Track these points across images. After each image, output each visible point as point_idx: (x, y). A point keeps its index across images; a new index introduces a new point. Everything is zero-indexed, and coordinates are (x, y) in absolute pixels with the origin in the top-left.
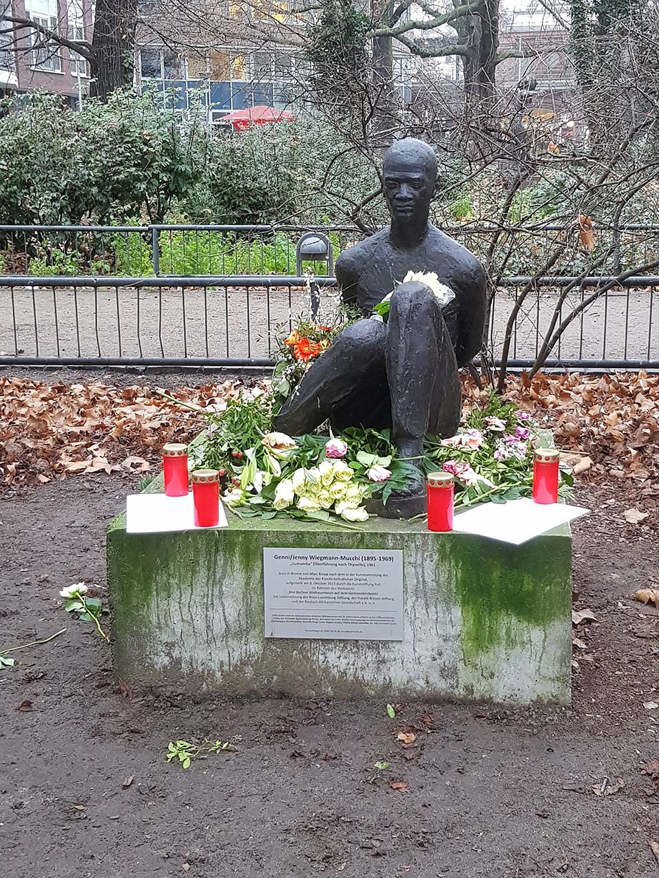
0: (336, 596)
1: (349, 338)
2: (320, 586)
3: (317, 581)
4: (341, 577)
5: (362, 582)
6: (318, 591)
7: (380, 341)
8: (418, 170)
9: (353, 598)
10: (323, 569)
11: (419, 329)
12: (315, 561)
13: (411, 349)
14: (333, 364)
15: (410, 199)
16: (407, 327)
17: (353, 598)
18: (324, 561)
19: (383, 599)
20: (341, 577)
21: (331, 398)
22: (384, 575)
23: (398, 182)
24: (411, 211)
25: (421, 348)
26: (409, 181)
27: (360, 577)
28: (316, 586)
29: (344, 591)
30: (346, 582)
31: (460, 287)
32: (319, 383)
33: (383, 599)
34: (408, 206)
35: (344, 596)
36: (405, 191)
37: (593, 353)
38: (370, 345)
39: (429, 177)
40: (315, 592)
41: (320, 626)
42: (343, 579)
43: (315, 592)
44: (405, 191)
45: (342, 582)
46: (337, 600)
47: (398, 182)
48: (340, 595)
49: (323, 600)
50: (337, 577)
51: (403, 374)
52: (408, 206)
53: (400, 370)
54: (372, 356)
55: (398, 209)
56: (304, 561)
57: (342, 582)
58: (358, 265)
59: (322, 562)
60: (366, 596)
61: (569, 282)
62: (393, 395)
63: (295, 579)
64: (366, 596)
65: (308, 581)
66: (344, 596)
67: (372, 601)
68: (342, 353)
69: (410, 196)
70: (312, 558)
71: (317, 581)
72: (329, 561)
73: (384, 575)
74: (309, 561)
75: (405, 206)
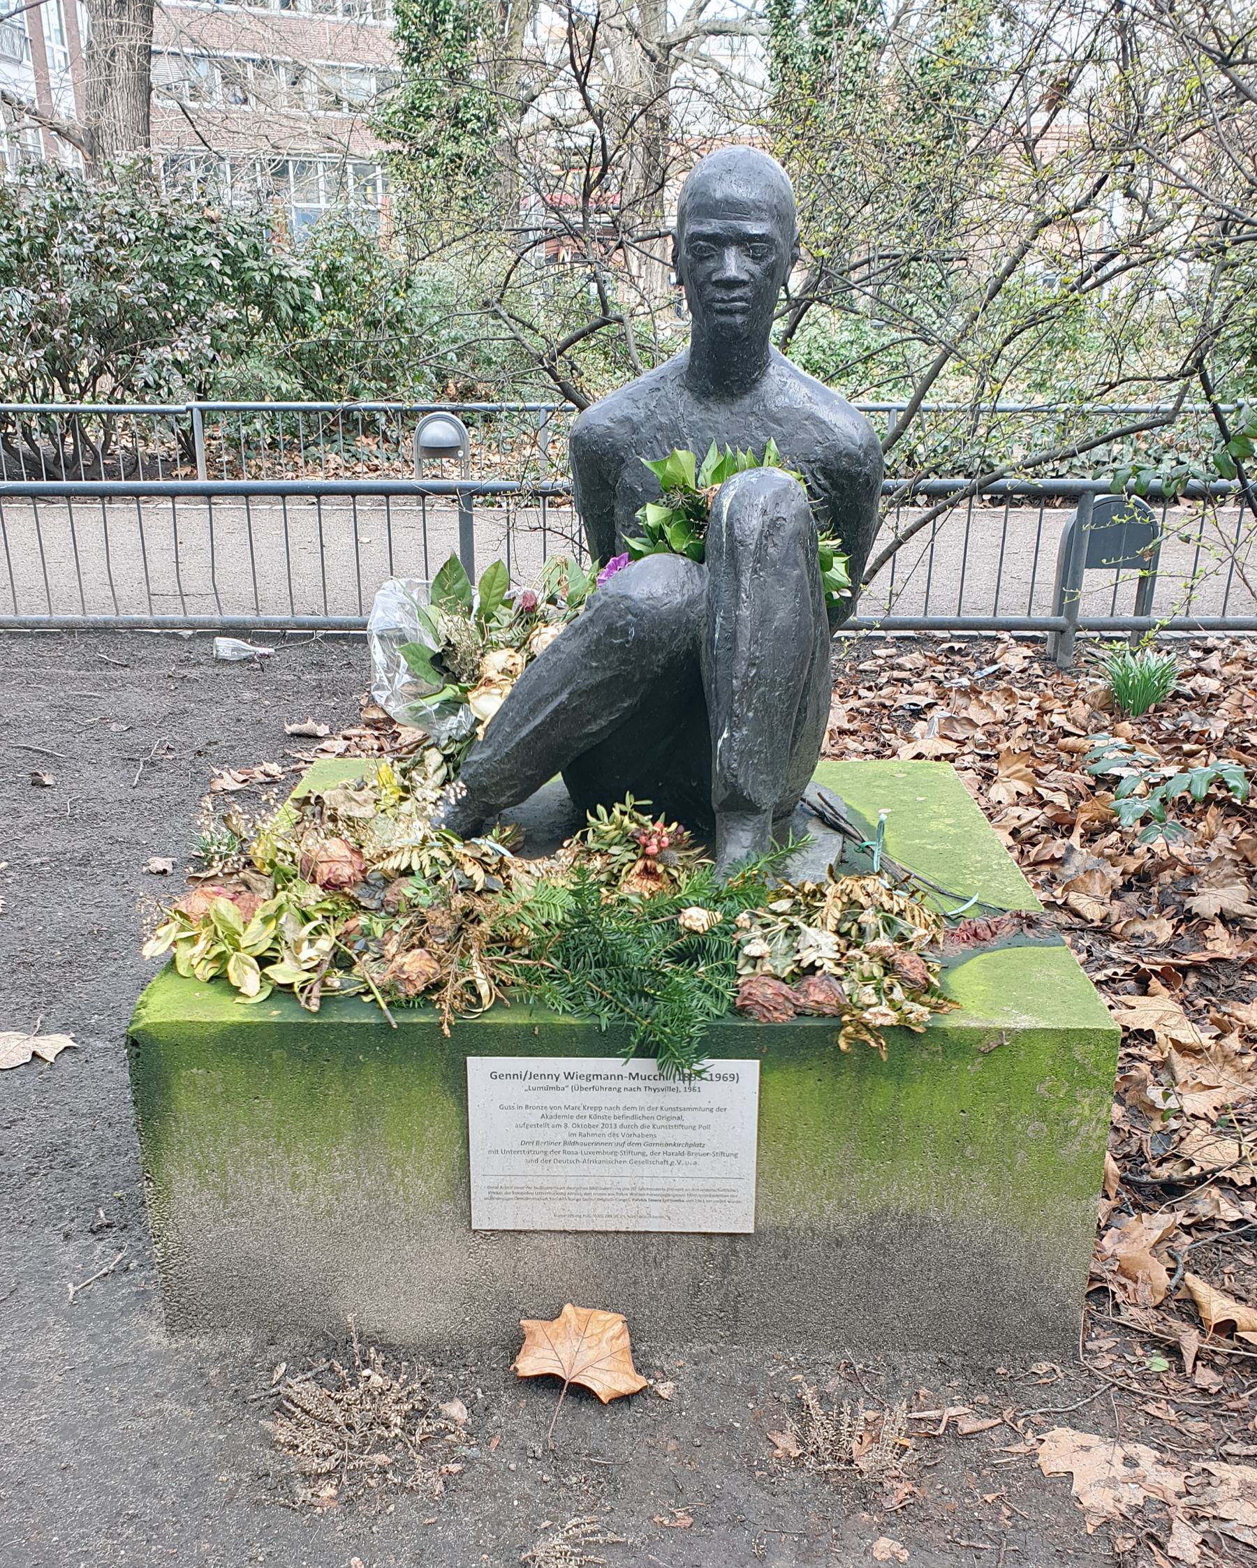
0: (618, 1149)
1: (625, 597)
2: (584, 1131)
3: (580, 1121)
4: (629, 1113)
5: (673, 1123)
6: (579, 1139)
7: (691, 603)
8: (763, 215)
9: (652, 1153)
10: (591, 1098)
11: (780, 577)
12: (575, 1082)
13: (763, 620)
14: (590, 653)
15: (743, 283)
16: (755, 571)
17: (652, 1153)
18: (595, 1082)
19: (715, 1154)
20: (629, 1113)
21: (583, 726)
22: (719, 1109)
23: (719, 241)
24: (743, 311)
25: (782, 616)
26: (744, 241)
27: (669, 1114)
28: (577, 1130)
29: (635, 1140)
30: (639, 1123)
31: (834, 485)
32: (556, 694)
33: (715, 1154)
34: (741, 299)
35: (635, 1149)
36: (734, 264)
37: (907, 610)
38: (670, 612)
39: (783, 236)
40: (575, 1143)
41: (585, 1208)
42: (634, 1117)
43: (575, 1143)
44: (734, 264)
45: (632, 1122)
46: (619, 1158)
47: (719, 241)
48: (626, 1148)
49: (592, 1157)
50: (621, 1113)
51: (746, 675)
52: (741, 299)
53: (741, 667)
54: (673, 636)
55: (718, 305)
56: (551, 1082)
57: (632, 1122)
58: (622, 433)
59: (589, 1085)
60: (681, 1149)
61: (954, 489)
62: (716, 714)
63: (535, 1117)
64: (681, 1149)
65: (562, 1121)
66: (635, 1149)
67: (692, 1159)
68: (611, 631)
69: (744, 277)
70: (569, 1076)
71: (580, 1121)
72: (606, 1084)
73: (719, 1109)
74: (563, 1082)
75: (734, 300)
